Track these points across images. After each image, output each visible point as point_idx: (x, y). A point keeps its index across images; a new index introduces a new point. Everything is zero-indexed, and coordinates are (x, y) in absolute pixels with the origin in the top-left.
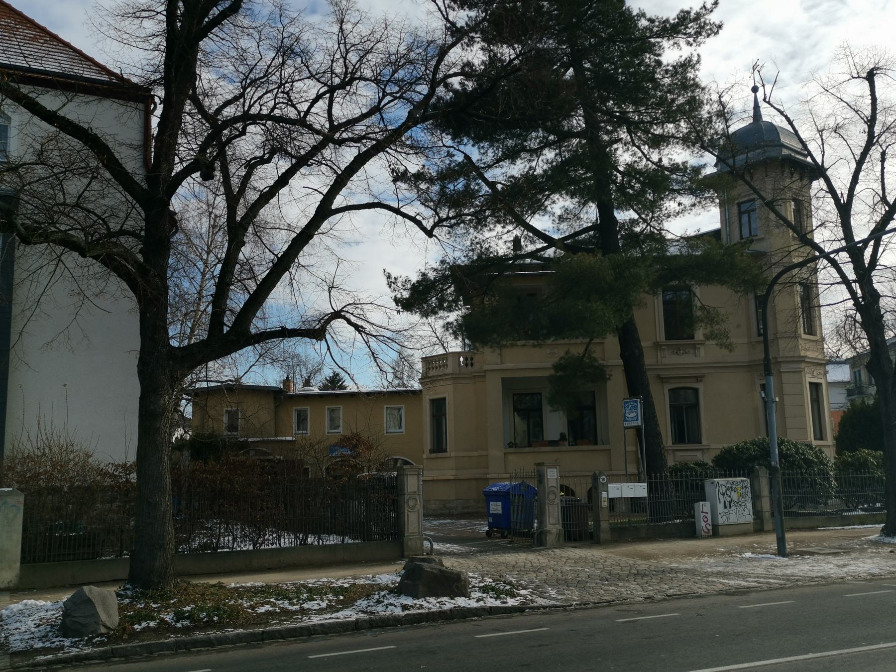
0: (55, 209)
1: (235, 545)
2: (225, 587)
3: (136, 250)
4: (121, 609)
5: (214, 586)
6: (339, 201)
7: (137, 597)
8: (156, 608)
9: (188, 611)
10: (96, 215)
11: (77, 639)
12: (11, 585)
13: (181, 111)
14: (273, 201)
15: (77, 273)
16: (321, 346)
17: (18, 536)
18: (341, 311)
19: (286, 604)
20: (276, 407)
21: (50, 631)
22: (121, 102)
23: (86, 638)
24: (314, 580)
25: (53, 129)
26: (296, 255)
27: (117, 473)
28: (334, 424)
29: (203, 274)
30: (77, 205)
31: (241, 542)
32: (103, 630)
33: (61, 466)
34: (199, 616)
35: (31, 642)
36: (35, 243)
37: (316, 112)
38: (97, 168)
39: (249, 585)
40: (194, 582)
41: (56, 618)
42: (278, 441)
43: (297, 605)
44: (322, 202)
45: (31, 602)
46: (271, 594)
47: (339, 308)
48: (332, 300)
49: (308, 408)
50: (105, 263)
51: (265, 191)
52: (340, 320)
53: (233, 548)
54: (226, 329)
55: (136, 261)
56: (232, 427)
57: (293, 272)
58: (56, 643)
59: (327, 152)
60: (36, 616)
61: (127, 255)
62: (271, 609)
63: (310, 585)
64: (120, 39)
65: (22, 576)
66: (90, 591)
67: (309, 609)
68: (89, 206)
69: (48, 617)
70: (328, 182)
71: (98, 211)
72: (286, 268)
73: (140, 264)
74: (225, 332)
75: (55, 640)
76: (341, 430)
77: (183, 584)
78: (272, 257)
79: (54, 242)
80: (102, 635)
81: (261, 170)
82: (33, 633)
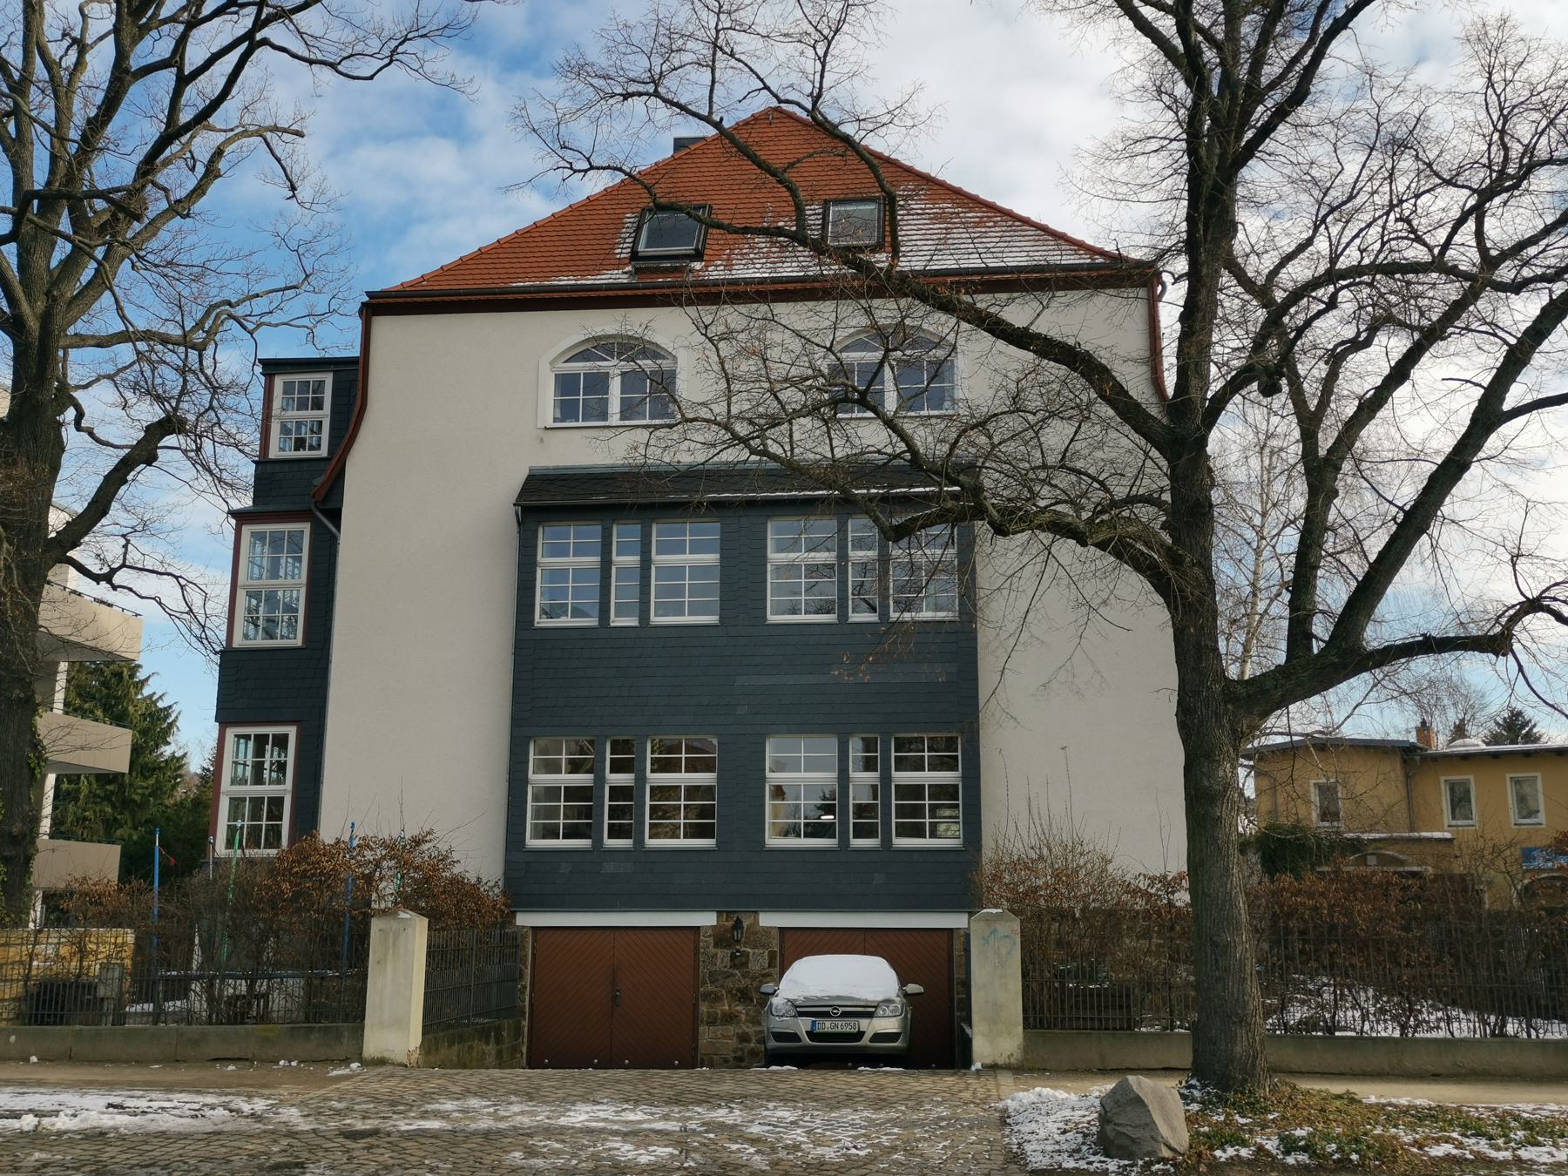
0: (1031, 475)
1: (1367, 1027)
2: (1360, 1102)
3: (1157, 526)
4: (1190, 1120)
5: (1339, 1097)
6: (1515, 395)
7: (1210, 1102)
8: (1246, 1125)
9: (1303, 1138)
10: (1089, 476)
11: (1126, 1162)
12: (1013, 1060)
13: (1214, 288)
14: (1382, 413)
15: (1077, 569)
16: (1506, 664)
17: (1016, 985)
18: (1540, 597)
19: (1483, 1146)
20: (1407, 776)
21: (1084, 1144)
22: (1111, 291)
23: (1140, 1162)
24: (1530, 1107)
25: (1030, 356)
26: (1439, 503)
27: (1153, 891)
28: (1526, 808)
29: (1258, 552)
30: (1062, 465)
31: (1378, 1022)
32: (1166, 1153)
33: (1068, 876)
34: (1323, 1148)
35: (1057, 1158)
36: (1015, 533)
37: (1460, 241)
38: (1090, 403)
39: (1404, 1101)
40: (1305, 1085)
41: (1089, 1122)
42: (1420, 840)
43: (1506, 1150)
44: (1483, 401)
45: (1047, 1091)
46: (1451, 1122)
47: (1536, 594)
48: (1520, 580)
49: (1470, 778)
50: (1118, 555)
51: (1368, 396)
52: (1539, 614)
53: (1362, 1031)
54: (1316, 647)
55: (1162, 544)
56: (1328, 814)
57: (1436, 534)
58: (1095, 1165)
59: (1483, 305)
60: (1059, 1116)
61: (1147, 536)
62: (1455, 1152)
63: (1525, 1115)
64: (1111, 196)
65: (1027, 1047)
66: (1139, 1083)
67: (1534, 1162)
68: (1079, 465)
69: (1076, 1119)
70: (1491, 362)
71: (1092, 471)
72: (1422, 529)
73: (1169, 549)
74: (1316, 651)
75: (1092, 1158)
76: (1542, 817)
77: (1284, 1088)
78: (1394, 510)
79: (1040, 527)
80: (1164, 1160)
81: (1356, 360)
82: (1058, 1143)
